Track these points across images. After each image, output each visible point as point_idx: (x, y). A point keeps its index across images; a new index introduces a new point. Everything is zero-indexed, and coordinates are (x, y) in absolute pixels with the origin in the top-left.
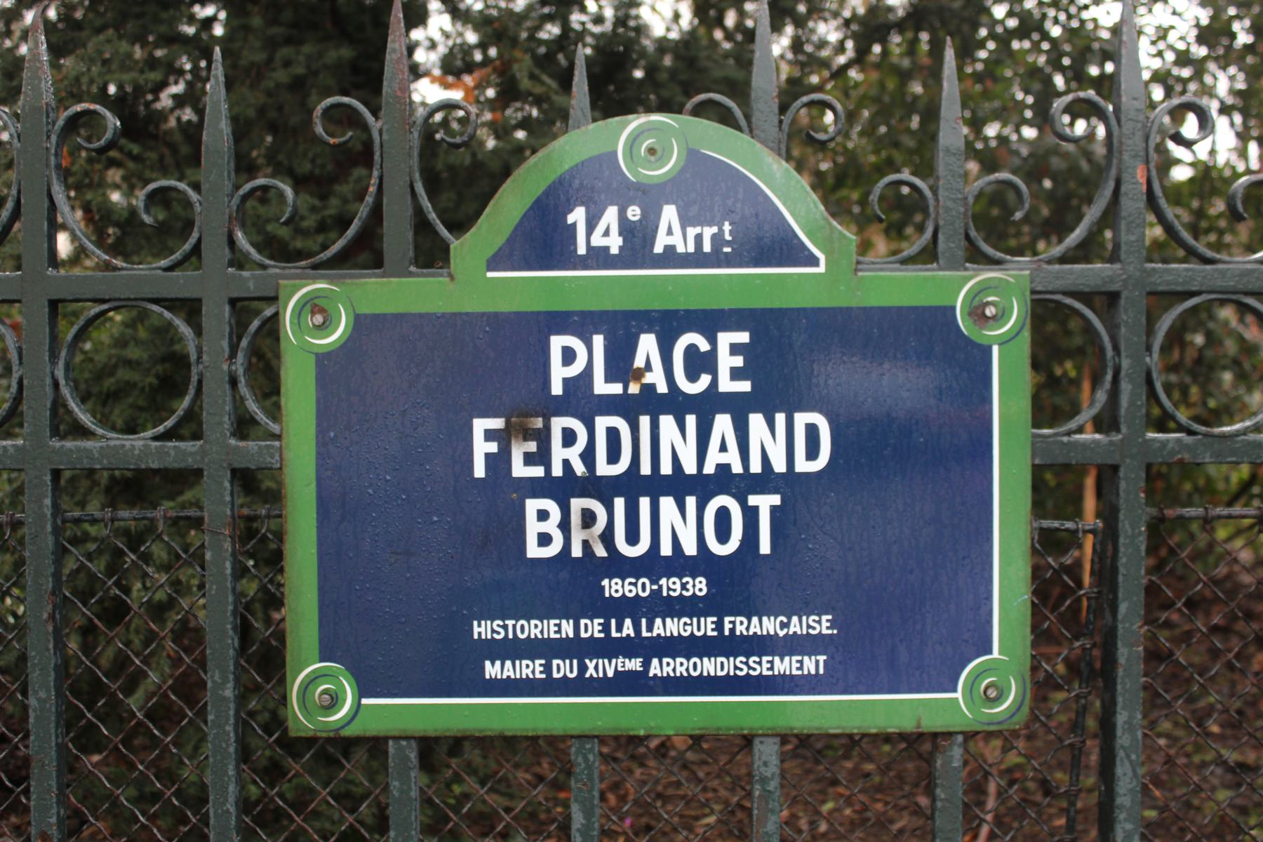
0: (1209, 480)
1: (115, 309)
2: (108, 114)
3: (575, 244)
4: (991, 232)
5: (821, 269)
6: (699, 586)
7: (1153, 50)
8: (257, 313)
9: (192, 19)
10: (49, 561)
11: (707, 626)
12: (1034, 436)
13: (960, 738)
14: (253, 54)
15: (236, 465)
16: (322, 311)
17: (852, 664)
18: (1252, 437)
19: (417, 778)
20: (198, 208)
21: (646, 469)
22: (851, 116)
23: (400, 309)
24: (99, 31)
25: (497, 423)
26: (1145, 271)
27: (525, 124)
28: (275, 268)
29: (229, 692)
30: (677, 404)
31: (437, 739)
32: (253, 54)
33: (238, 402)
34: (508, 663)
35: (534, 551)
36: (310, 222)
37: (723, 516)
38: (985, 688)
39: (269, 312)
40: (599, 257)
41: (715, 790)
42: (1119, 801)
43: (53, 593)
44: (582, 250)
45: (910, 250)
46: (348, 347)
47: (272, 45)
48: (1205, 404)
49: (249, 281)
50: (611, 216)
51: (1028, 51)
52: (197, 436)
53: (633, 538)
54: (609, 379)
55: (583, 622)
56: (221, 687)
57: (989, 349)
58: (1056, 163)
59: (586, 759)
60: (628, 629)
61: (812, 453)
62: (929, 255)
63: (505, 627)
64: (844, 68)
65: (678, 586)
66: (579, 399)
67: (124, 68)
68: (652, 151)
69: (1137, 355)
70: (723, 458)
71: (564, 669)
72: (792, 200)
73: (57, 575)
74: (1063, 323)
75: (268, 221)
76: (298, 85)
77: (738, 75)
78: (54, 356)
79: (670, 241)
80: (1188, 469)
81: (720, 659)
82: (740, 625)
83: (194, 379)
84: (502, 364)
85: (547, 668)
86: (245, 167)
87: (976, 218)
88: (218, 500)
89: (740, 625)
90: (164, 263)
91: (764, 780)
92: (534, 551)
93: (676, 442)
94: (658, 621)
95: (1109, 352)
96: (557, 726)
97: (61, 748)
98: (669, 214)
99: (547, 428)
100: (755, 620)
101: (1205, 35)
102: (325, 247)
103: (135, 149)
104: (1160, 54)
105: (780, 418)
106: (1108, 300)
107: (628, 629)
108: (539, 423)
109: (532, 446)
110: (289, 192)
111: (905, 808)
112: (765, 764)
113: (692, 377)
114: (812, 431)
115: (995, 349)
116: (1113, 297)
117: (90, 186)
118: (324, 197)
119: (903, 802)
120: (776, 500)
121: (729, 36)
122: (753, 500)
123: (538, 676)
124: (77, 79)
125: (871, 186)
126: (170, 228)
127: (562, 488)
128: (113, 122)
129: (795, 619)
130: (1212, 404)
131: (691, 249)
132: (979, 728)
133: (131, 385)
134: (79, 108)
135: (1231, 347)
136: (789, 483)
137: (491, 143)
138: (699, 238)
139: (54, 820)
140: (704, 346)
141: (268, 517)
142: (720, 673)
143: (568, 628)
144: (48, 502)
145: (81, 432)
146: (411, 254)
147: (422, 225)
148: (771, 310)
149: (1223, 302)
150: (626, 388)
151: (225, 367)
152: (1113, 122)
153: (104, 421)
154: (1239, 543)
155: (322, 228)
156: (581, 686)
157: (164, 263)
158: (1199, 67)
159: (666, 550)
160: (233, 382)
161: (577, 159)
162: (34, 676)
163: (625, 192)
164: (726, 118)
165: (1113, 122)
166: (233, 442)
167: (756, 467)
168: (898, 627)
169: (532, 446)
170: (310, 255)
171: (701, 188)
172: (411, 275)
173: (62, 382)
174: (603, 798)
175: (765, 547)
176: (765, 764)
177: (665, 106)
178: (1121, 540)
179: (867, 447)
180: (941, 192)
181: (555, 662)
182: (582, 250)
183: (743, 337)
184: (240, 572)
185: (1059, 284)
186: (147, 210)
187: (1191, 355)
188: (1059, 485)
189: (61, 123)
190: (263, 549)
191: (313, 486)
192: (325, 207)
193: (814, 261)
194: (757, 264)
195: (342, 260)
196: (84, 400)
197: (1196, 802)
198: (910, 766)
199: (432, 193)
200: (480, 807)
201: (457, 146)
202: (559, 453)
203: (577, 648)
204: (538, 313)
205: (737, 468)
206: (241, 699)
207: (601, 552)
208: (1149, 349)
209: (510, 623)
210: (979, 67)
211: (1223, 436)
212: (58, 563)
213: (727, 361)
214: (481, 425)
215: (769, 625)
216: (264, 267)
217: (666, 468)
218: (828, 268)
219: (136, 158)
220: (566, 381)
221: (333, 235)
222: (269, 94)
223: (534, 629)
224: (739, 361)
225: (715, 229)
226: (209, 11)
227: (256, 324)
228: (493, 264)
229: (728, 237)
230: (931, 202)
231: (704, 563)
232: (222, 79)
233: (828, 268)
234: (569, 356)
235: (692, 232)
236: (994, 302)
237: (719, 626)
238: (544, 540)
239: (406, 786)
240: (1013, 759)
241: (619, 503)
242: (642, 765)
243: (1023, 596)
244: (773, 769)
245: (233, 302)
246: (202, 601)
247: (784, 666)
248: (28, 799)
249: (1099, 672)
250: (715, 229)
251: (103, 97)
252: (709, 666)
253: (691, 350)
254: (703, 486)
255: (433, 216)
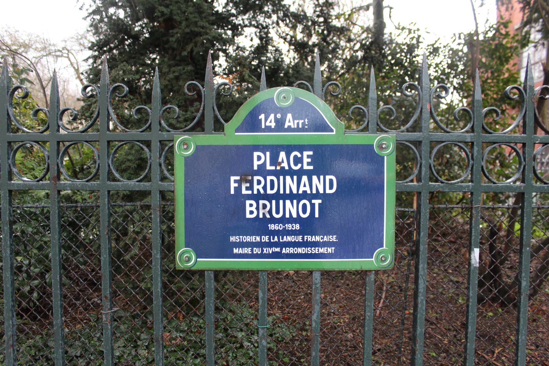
0: (450, 198)
1: (125, 144)
2: (125, 86)
3: (261, 125)
4: (386, 123)
5: (334, 133)
6: (297, 227)
7: (435, 70)
8: (166, 145)
9: (149, 59)
10: (107, 217)
11: (300, 238)
12: (397, 183)
13: (374, 272)
14: (165, 70)
15: (161, 190)
16: (186, 144)
17: (342, 250)
18: (460, 184)
19: (213, 284)
20: (150, 114)
21: (282, 192)
22: (345, 88)
23: (210, 144)
24: (122, 62)
25: (238, 178)
26: (429, 135)
27: (247, 89)
28: (173, 132)
29: (158, 256)
30: (291, 173)
31: (220, 271)
32: (165, 70)
33: (162, 172)
34: (240, 249)
35: (248, 216)
36: (181, 119)
37: (304, 206)
38: (381, 257)
39: (171, 145)
40: (268, 129)
41: (302, 289)
42: (419, 290)
43: (108, 227)
44: (263, 127)
45: (361, 128)
46: (194, 155)
47: (170, 66)
48: (449, 175)
49: (165, 135)
50: (272, 117)
51: (398, 70)
52: (150, 181)
53: (278, 212)
54: (271, 165)
55: (263, 237)
56: (156, 254)
57: (384, 157)
58: (406, 103)
59: (263, 278)
60: (276, 239)
61: (331, 187)
62: (366, 129)
63: (240, 238)
64: (343, 74)
65: (291, 227)
66: (262, 171)
67: (130, 74)
68: (285, 98)
69: (427, 160)
70: (305, 189)
71: (257, 251)
72: (326, 112)
73: (109, 221)
74: (408, 151)
75: (170, 118)
76: (177, 78)
77: (310, 75)
78: (108, 157)
79: (289, 124)
80: (444, 194)
81: (303, 248)
82: (309, 238)
83: (149, 164)
84: (239, 160)
85: (252, 250)
86: (164, 102)
87: (380, 118)
88: (155, 200)
89: (309, 238)
90: (140, 130)
91: (316, 284)
92: (248, 216)
93: (291, 184)
94: (285, 237)
95: (419, 159)
96: (255, 268)
97: (111, 272)
98: (289, 116)
99: (253, 179)
100: (314, 237)
101: (449, 66)
102: (186, 126)
103: (132, 97)
104: (437, 71)
105: (322, 177)
106: (418, 143)
107: (276, 239)
108: (250, 178)
109: (248, 185)
110: (177, 109)
111: (359, 294)
112: (316, 279)
113: (296, 165)
114: (331, 181)
115: (385, 157)
116: (420, 142)
117: (119, 108)
118: (186, 111)
119: (358, 292)
120: (320, 201)
121: (309, 64)
122: (313, 201)
123: (249, 253)
124: (115, 77)
125: (350, 110)
126: (141, 121)
127: (257, 197)
128: (126, 89)
129: (325, 237)
130: (452, 175)
131: (296, 127)
132: (379, 269)
133: (130, 167)
134: (116, 85)
135: (457, 158)
136: (324, 196)
137: (237, 96)
138: (298, 124)
139: (108, 292)
140: (299, 155)
141: (170, 205)
142: (303, 252)
143: (258, 239)
144: (106, 200)
145: (115, 180)
146: (213, 127)
147: (216, 120)
148: (319, 145)
149: (456, 145)
150: (276, 168)
151: (158, 161)
152: (420, 91)
153: (122, 177)
154: (459, 217)
155: (186, 120)
156: (262, 256)
157: (140, 130)
158: (448, 75)
159: (287, 216)
160: (160, 165)
161: (262, 100)
162: (103, 250)
163: (276, 110)
164: (308, 89)
165: (420, 91)
166: (160, 183)
167: (314, 191)
168: (357, 239)
169: (248, 185)
170: (181, 128)
171: (299, 109)
172: (212, 134)
173: (111, 165)
174: (269, 290)
175: (317, 215)
176: (316, 279)
177: (290, 84)
178: (422, 214)
179: (348, 188)
180: (370, 111)
181: (254, 249)
182: (263, 127)
183: (311, 153)
184: (162, 222)
185: (404, 138)
186: (136, 115)
187: (445, 160)
188: (407, 199)
189: (111, 89)
190: (168, 217)
191: (183, 196)
192: (186, 115)
193: (332, 131)
194: (315, 132)
195: (193, 129)
196: (117, 170)
197: (444, 293)
198: (360, 282)
199: (219, 110)
200: (232, 292)
201: (227, 96)
202: (256, 187)
203: (260, 245)
204: (250, 145)
205: (309, 192)
206: (162, 259)
207: (268, 216)
208: (430, 158)
209: (241, 237)
210: (383, 74)
211: (452, 184)
212: (109, 218)
213: (306, 160)
214: (233, 178)
215: (318, 238)
216: (169, 131)
217: (288, 192)
218: (337, 133)
219: (131, 100)
220: (258, 165)
221: (188, 123)
222: (169, 81)
223: (248, 239)
224: (309, 160)
225: (303, 121)
226: (155, 56)
227: (167, 148)
228: (237, 130)
229: (307, 123)
230: (367, 114)
231: (299, 220)
232: (158, 76)
233: (337, 133)
234: (259, 158)
235: (296, 122)
236: (385, 143)
237: (303, 239)
238: (251, 212)
239: (210, 285)
240: (391, 280)
241: (274, 202)
242: (281, 281)
243: (393, 230)
244: (318, 281)
245: (160, 141)
246: (150, 231)
247: (322, 250)
248: (101, 286)
249: (415, 253)
250: (303, 121)
251: (123, 81)
252: (300, 250)
253: (295, 157)
254: (298, 197)
255: (219, 116)
